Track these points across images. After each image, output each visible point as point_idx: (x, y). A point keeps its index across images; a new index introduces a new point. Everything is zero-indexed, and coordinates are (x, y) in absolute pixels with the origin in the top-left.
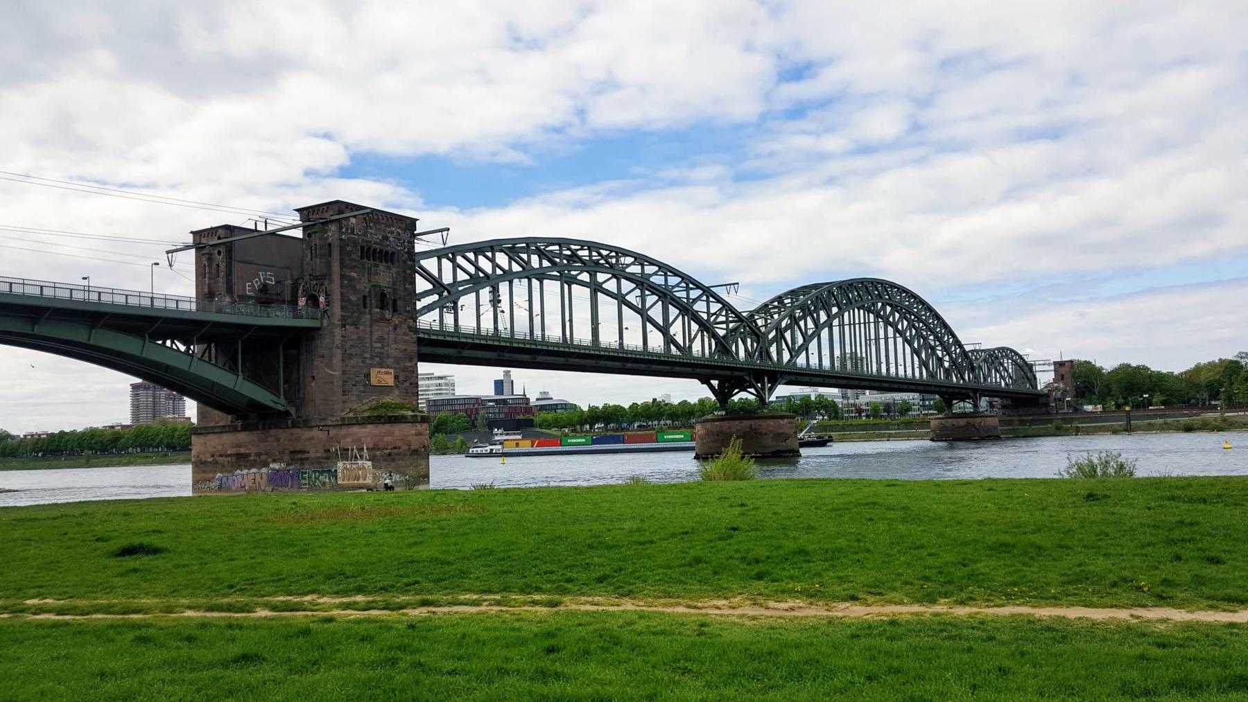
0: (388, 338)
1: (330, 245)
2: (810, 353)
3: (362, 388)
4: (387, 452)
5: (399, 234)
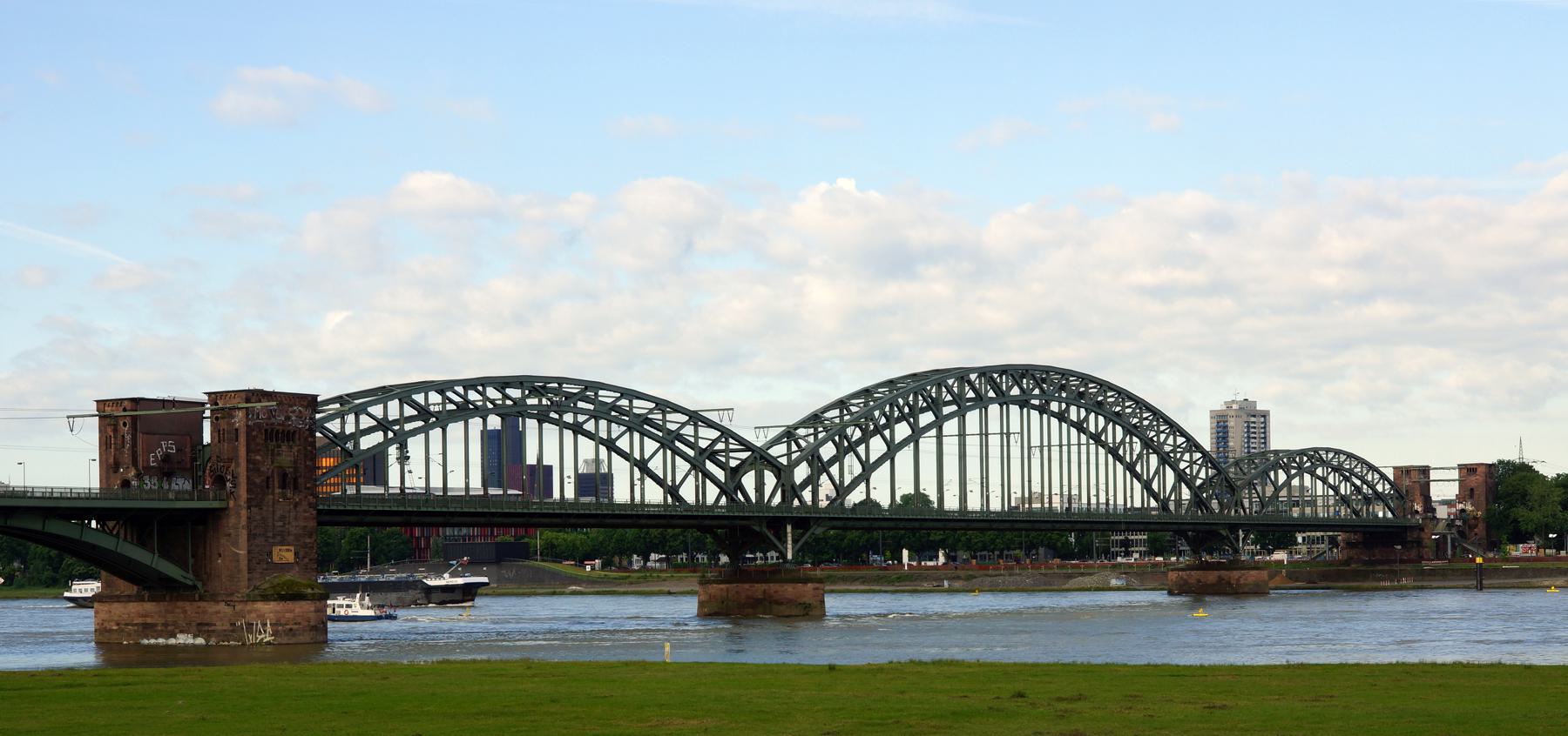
0: (289, 517)
1: (237, 430)
2: (871, 486)
4: (288, 627)
5: (300, 411)
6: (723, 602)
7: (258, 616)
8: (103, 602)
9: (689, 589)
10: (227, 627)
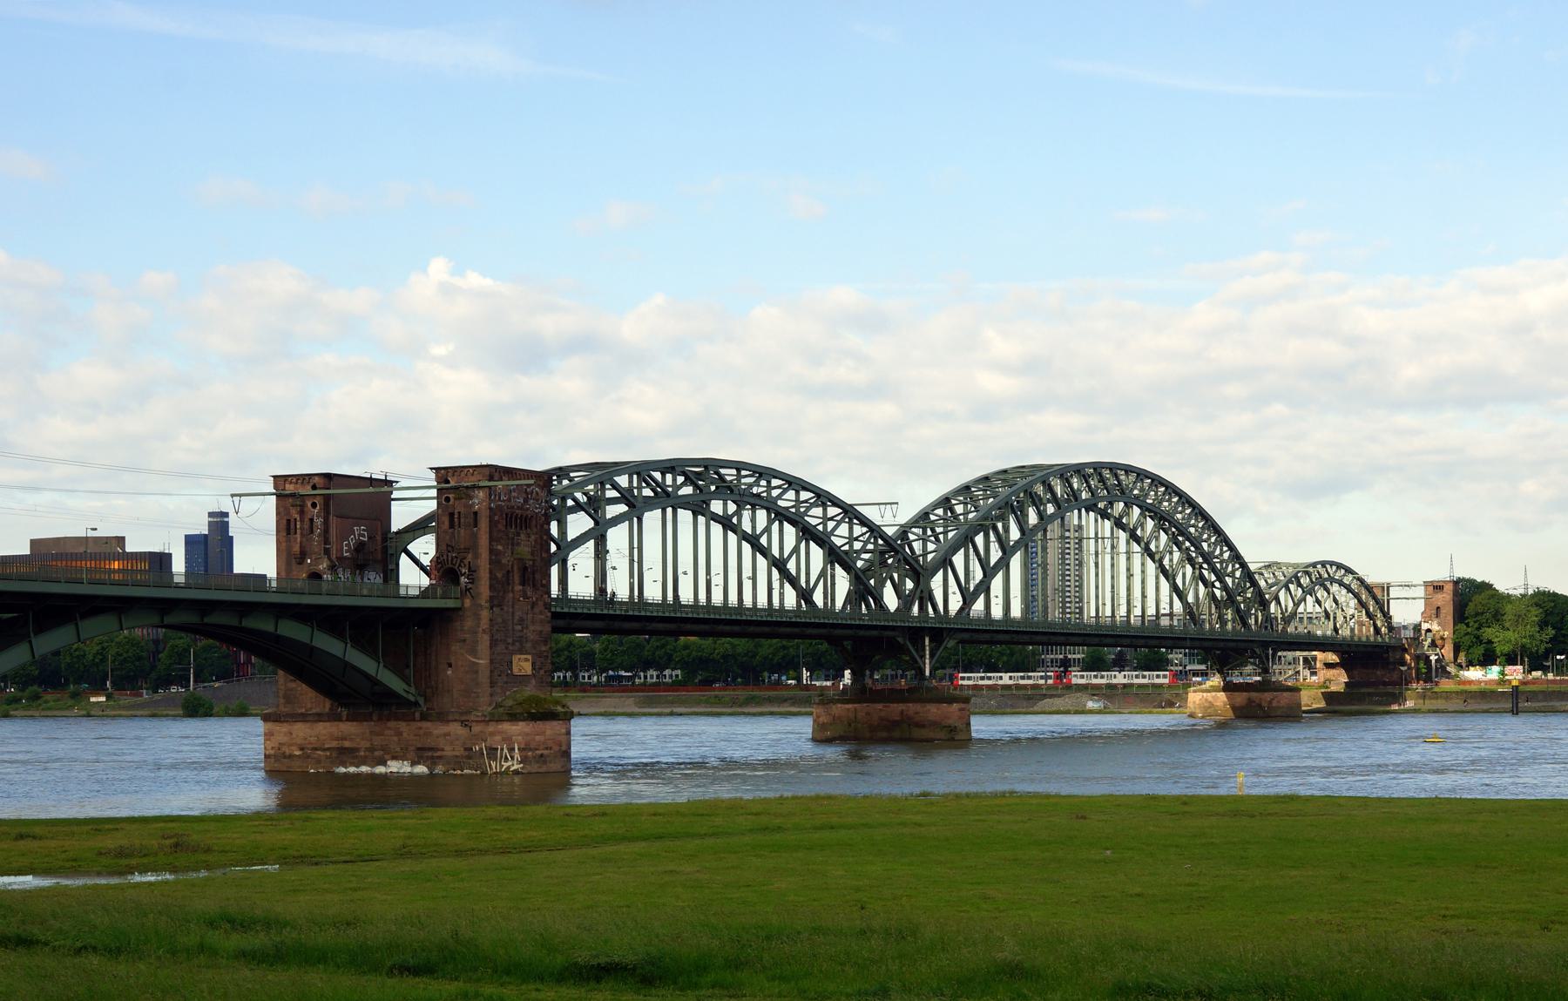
3: (505, 679)
6: (850, 725)
7: (504, 740)
8: (280, 721)
9: (602, 710)
10: (460, 752)
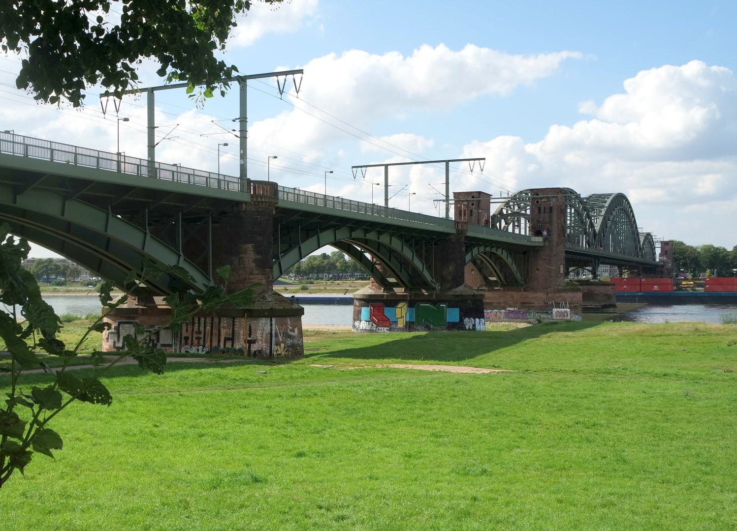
4: (575, 305)
10: (542, 304)
